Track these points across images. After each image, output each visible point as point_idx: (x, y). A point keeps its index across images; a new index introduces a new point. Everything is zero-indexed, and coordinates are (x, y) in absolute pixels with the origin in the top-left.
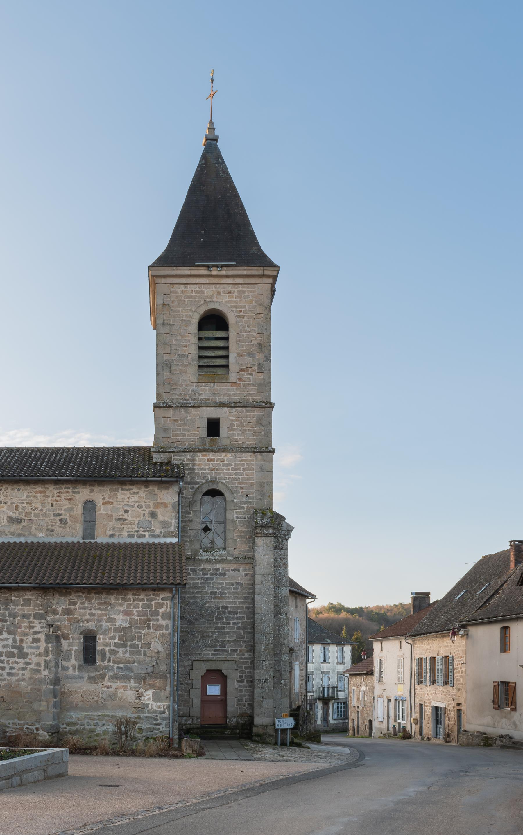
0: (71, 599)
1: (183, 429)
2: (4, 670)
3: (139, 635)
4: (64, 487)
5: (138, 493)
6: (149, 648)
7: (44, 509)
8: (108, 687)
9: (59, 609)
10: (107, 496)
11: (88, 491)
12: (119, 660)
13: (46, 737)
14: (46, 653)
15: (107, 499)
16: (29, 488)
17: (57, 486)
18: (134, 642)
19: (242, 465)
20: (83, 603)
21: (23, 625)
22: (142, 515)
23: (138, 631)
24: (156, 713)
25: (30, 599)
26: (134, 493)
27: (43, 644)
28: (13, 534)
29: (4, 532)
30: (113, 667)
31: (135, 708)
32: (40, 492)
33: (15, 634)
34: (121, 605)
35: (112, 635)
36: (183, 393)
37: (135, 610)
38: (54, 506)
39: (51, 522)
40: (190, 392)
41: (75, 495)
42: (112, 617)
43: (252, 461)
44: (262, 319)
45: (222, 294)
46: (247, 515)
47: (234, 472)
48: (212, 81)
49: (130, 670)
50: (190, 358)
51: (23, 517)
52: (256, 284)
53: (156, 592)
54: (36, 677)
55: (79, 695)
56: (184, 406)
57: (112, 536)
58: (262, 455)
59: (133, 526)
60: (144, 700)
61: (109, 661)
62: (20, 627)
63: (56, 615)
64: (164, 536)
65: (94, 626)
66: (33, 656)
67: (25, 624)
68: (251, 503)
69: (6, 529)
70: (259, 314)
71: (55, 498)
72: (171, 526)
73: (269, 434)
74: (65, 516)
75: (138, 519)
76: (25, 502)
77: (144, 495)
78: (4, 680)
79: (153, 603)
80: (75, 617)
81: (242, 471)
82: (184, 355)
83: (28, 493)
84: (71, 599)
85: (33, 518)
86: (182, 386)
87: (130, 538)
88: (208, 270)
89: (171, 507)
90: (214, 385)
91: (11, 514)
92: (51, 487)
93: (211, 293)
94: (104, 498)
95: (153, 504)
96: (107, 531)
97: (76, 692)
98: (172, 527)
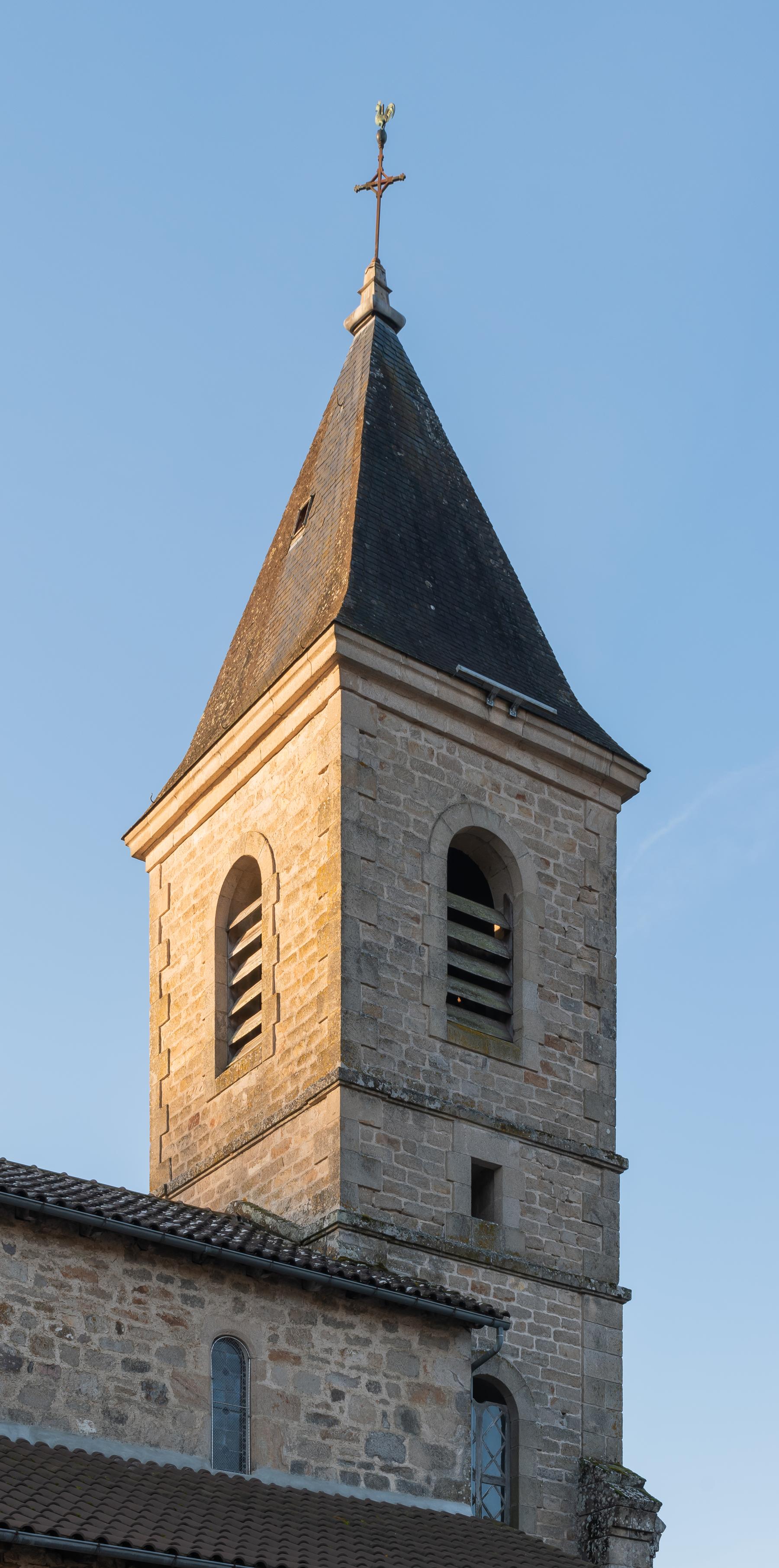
1: (411, 1175)
4: (156, 1272)
5: (367, 1342)
7: (95, 1337)
10: (281, 1330)
11: (230, 1304)
15: (282, 1345)
16: (43, 1250)
17: (136, 1267)
19: (554, 1322)
22: (379, 1418)
26: (358, 1340)
32: (80, 1274)
36: (409, 1064)
38: (126, 1335)
39: (117, 1387)
40: (427, 1067)
41: (189, 1309)
43: (575, 1314)
44: (596, 907)
45: (503, 794)
46: (564, 1472)
47: (535, 1338)
48: (383, 140)
50: (425, 959)
51: (25, 1351)
56: (415, 1104)
57: (298, 1468)
58: (598, 1304)
59: (354, 1445)
64: (438, 1495)
68: (572, 1436)
70: (590, 889)
72: (454, 1464)
73: (612, 1248)
75: (369, 1427)
76: (31, 1299)
81: (552, 1339)
82: (413, 945)
83: (41, 1267)
85: (57, 1361)
86: (407, 1041)
87: (348, 1483)
88: (485, 704)
89: (453, 1405)
90: (484, 1065)
92: (116, 1264)
93: (477, 780)
94: (274, 1339)
95: (408, 1385)
98: (458, 1470)
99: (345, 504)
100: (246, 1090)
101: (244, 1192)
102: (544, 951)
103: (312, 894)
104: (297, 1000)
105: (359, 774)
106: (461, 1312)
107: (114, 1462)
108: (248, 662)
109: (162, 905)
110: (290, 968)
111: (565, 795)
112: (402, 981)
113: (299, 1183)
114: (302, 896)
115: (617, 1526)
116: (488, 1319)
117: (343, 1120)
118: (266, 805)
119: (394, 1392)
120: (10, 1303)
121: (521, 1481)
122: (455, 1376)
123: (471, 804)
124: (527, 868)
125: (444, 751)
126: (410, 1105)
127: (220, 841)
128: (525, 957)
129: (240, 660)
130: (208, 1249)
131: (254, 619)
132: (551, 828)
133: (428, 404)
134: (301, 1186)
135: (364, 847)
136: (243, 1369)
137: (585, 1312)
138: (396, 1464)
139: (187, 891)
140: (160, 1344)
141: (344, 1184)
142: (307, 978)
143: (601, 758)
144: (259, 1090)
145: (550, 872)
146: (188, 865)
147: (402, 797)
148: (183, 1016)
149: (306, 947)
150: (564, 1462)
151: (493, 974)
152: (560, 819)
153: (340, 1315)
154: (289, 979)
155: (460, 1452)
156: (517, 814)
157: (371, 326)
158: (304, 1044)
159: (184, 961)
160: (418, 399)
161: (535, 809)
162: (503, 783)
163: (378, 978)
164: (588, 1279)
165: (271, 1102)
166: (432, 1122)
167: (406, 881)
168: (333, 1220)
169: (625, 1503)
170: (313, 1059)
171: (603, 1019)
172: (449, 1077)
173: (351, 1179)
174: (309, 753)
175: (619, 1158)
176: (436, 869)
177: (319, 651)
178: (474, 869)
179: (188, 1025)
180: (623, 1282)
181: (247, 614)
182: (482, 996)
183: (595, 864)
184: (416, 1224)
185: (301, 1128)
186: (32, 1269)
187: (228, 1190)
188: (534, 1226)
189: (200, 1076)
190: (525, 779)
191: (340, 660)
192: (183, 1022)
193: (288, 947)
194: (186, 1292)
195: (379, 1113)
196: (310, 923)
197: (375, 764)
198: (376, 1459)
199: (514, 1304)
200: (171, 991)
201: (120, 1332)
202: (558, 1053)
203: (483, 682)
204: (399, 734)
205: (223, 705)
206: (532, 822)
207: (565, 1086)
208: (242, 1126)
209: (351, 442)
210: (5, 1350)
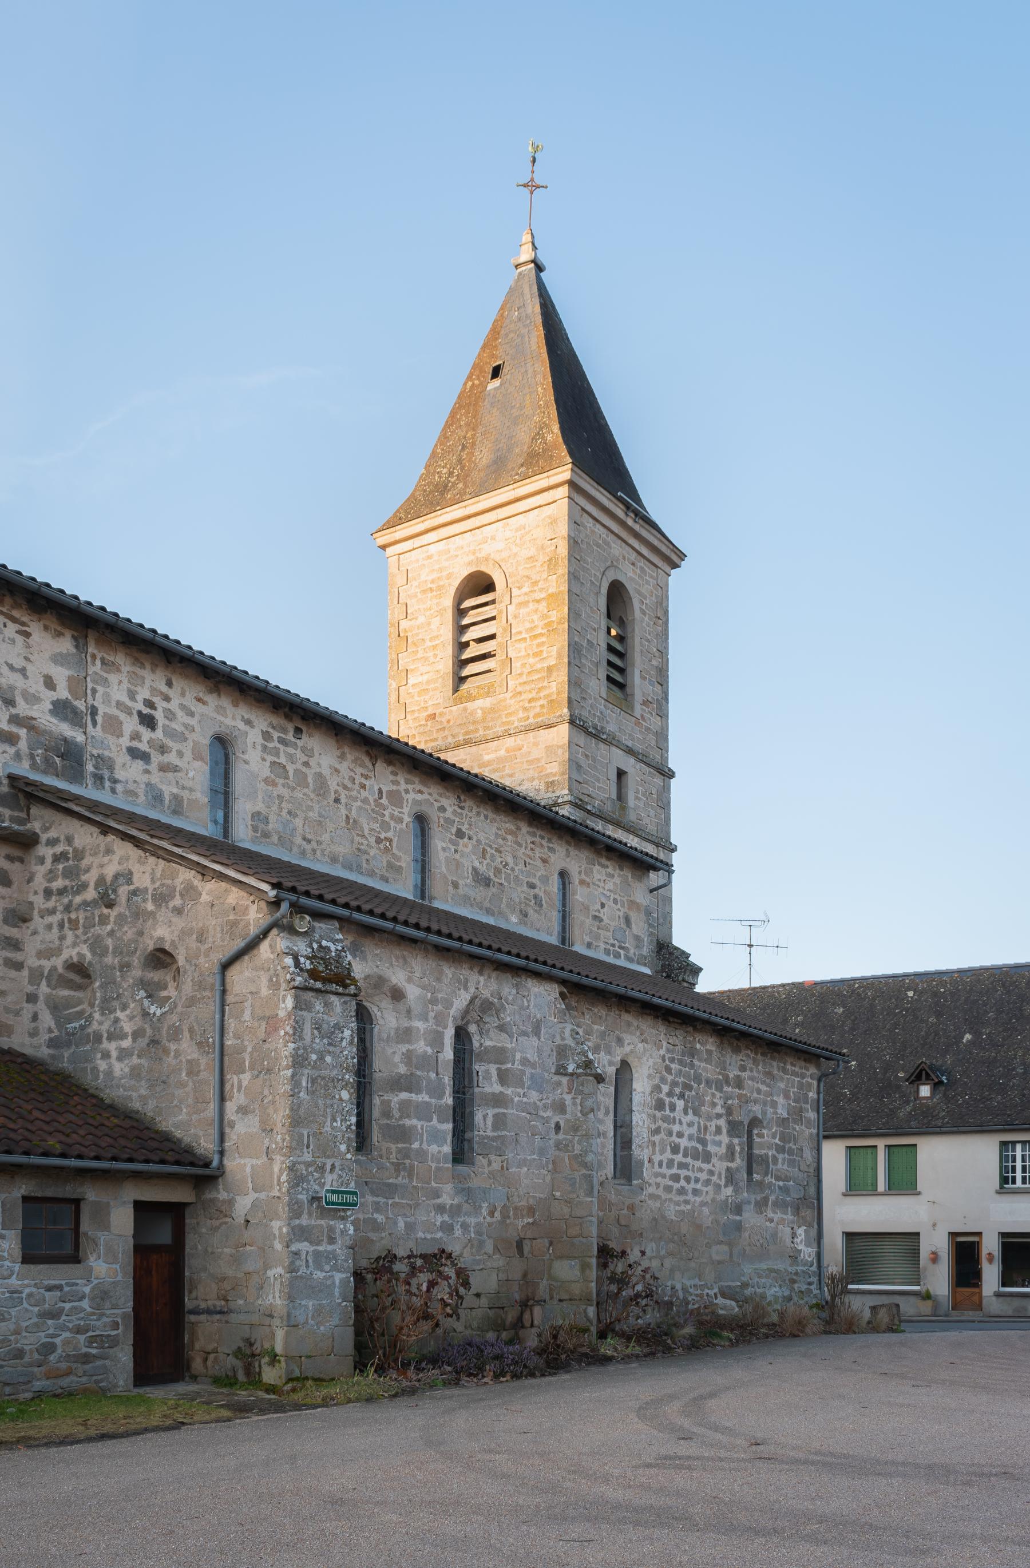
4: (539, 833)
7: (516, 868)
8: (771, 1220)
13: (733, 1309)
14: (730, 1155)
15: (583, 877)
16: (498, 818)
17: (531, 830)
20: (751, 1070)
27: (724, 1138)
32: (511, 833)
33: (700, 1116)
34: (782, 1079)
48: (534, 161)
54: (718, 1198)
69: (472, 893)
78: (687, 1202)
91: (477, 864)
99: (539, 378)
100: (481, 709)
102: (642, 652)
109: (400, 580)
113: (531, 772)
139: (423, 578)
140: (539, 874)
145: (644, 607)
146: (426, 562)
149: (535, 637)
153: (604, 861)
156: (629, 575)
159: (422, 619)
161: (638, 571)
162: (627, 556)
165: (504, 720)
166: (602, 745)
168: (566, 799)
171: (663, 692)
175: (670, 770)
186: (494, 829)
191: (571, 483)
192: (419, 655)
195: (582, 739)
200: (409, 634)
209: (534, 340)
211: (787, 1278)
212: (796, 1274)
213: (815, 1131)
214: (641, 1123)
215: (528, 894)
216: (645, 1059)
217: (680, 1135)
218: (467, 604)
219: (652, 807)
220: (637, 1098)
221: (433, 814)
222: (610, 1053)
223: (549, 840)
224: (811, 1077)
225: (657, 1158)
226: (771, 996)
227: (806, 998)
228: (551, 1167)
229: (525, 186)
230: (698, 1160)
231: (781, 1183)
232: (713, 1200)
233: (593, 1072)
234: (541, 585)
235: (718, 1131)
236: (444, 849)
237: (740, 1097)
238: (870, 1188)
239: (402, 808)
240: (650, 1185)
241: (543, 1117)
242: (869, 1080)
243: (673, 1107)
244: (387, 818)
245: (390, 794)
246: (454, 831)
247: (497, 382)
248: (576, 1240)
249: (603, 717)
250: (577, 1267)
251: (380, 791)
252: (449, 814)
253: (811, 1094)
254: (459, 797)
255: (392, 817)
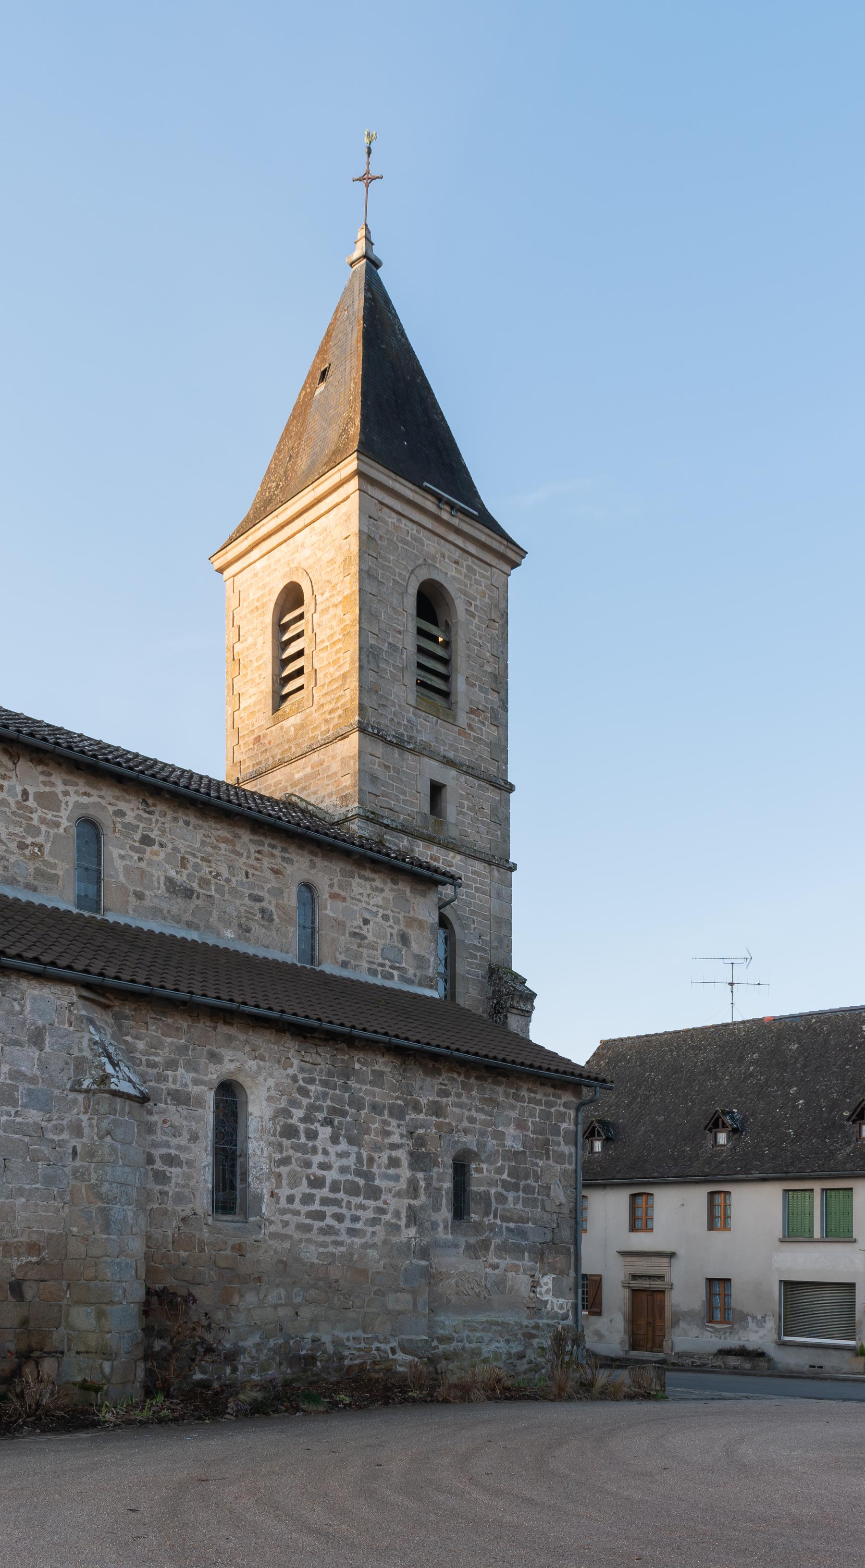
0: (441, 1084)
2: (343, 1221)
3: (536, 1168)
4: (267, 841)
5: (382, 890)
6: (548, 1196)
7: (234, 879)
8: (495, 1267)
9: (423, 1101)
11: (307, 863)
12: (509, 1214)
15: (336, 890)
16: (205, 825)
17: (256, 838)
18: (529, 1182)
19: (475, 881)
20: (459, 1095)
21: (373, 1126)
22: (389, 936)
23: (535, 1161)
24: (558, 1318)
25: (383, 1072)
27: (405, 1172)
28: (177, 920)
29: (161, 911)
30: (501, 1227)
31: (528, 1308)
32: (226, 841)
33: (360, 1146)
34: (513, 1107)
35: (499, 1164)
37: (530, 1120)
39: (246, 911)
40: (405, 722)
41: (286, 865)
42: (500, 1129)
43: (486, 877)
46: (480, 972)
48: (369, 152)
49: (523, 1234)
51: (195, 886)
52: (491, 566)
53: (557, 1091)
54: (395, 1239)
55: (452, 1282)
56: (399, 744)
57: (344, 964)
58: (499, 871)
59: (375, 952)
60: (541, 1294)
61: (495, 1217)
62: (368, 1131)
63: (419, 1114)
65: (475, 1143)
66: (390, 1196)
67: (377, 1125)
69: (165, 906)
70: (494, 621)
71: (251, 862)
72: (429, 966)
74: (270, 905)
75: (383, 942)
77: (391, 898)
78: (341, 1244)
79: (553, 1110)
80: (447, 1121)
81: (473, 891)
82: (398, 648)
83: (204, 835)
84: (441, 1084)
85: (213, 893)
86: (395, 707)
88: (438, 506)
90: (437, 723)
91: (172, 873)
92: (246, 836)
93: (433, 551)
95: (404, 917)
96: (337, 955)
97: (449, 1276)
98: (431, 970)
99: (354, 374)
100: (293, 725)
101: (292, 788)
102: (469, 656)
103: (339, 611)
104: (329, 675)
105: (368, 542)
106: (436, 876)
107: (245, 956)
108: (290, 460)
110: (324, 655)
111: (480, 563)
112: (392, 669)
113: (330, 787)
114: (332, 611)
115: (512, 1007)
116: (450, 881)
117: (360, 752)
118: (307, 552)
119: (397, 921)
120: (187, 856)
121: (457, 976)
122: (429, 913)
123: (429, 565)
124: (460, 605)
125: (414, 532)
126: (397, 745)
127: (275, 570)
128: (459, 659)
129: (284, 458)
130: (299, 830)
131: (293, 434)
132: (473, 583)
133: (396, 316)
134: (331, 789)
135: (371, 588)
136: (313, 902)
137: (492, 876)
138: (398, 965)
139: (251, 597)
140: (269, 886)
141: (360, 790)
142: (335, 662)
143: (501, 543)
144: (301, 727)
145: (472, 609)
147: (392, 558)
148: (249, 673)
149: (334, 643)
150: (479, 966)
151: (440, 668)
152: (477, 577)
153: (368, 873)
154: (322, 662)
155: (432, 959)
156: (454, 574)
157: (362, 266)
158: (333, 702)
159: (250, 640)
160: (391, 312)
161: (464, 570)
162: (447, 553)
163: (379, 667)
164: (494, 856)
165: (311, 735)
166: (409, 756)
167: (394, 609)
168: (355, 812)
169: (517, 993)
170: (340, 712)
171: (501, 700)
172: (417, 729)
173: (364, 788)
174: (337, 525)
175: (510, 784)
176: (411, 603)
177: (346, 466)
178: (431, 603)
179: (253, 680)
180: (512, 860)
181: (287, 429)
182: (435, 681)
183: (497, 606)
184: (399, 817)
185: (331, 753)
186: (199, 837)
187: (281, 786)
188: (464, 822)
189: (261, 713)
190: (459, 552)
191: (359, 473)
192: (249, 677)
193: (322, 641)
194: (284, 855)
195: (379, 749)
196: (337, 629)
197: (377, 537)
198: (387, 961)
199: (453, 869)
200: (241, 657)
201: (247, 877)
202: (476, 718)
203: (439, 494)
204: (390, 520)
205: (274, 485)
206: (462, 578)
207: (480, 739)
208: (290, 747)
209: (355, 335)
210: (184, 885)
211: (520, 1332)
212: (537, 1327)
213: (573, 1167)
214: (258, 1152)
215: (251, 908)
216: (261, 1078)
217: (324, 1166)
218: (287, 618)
219: (483, 823)
220: (253, 1124)
221: (106, 818)
222: (196, 1070)
223: (284, 850)
224: (565, 1105)
225: (284, 1192)
226: (732, 1033)
227: (764, 1034)
228: (67, 1198)
229: (360, 180)
230: (358, 1195)
231: (512, 1225)
232: (385, 1242)
233: (107, 1088)
234: (339, 588)
235: (394, 1163)
236: (122, 857)
237: (439, 1126)
238: (807, 1234)
239: (59, 811)
240: (271, 1223)
241: (53, 1141)
242: (814, 1119)
243: (312, 1135)
244: (35, 822)
245: (39, 796)
246: (138, 836)
247: (322, 387)
248: (92, 1284)
249: (411, 725)
250: (93, 1315)
251: (25, 793)
252: (130, 817)
253: (564, 1126)
254: (144, 801)
255: (43, 821)
